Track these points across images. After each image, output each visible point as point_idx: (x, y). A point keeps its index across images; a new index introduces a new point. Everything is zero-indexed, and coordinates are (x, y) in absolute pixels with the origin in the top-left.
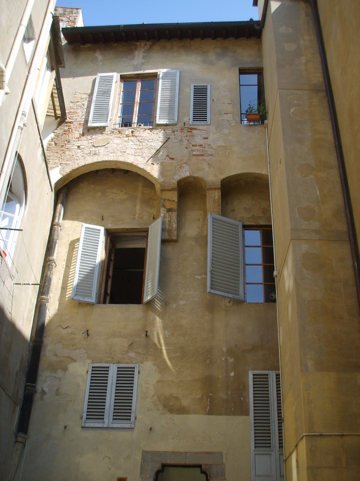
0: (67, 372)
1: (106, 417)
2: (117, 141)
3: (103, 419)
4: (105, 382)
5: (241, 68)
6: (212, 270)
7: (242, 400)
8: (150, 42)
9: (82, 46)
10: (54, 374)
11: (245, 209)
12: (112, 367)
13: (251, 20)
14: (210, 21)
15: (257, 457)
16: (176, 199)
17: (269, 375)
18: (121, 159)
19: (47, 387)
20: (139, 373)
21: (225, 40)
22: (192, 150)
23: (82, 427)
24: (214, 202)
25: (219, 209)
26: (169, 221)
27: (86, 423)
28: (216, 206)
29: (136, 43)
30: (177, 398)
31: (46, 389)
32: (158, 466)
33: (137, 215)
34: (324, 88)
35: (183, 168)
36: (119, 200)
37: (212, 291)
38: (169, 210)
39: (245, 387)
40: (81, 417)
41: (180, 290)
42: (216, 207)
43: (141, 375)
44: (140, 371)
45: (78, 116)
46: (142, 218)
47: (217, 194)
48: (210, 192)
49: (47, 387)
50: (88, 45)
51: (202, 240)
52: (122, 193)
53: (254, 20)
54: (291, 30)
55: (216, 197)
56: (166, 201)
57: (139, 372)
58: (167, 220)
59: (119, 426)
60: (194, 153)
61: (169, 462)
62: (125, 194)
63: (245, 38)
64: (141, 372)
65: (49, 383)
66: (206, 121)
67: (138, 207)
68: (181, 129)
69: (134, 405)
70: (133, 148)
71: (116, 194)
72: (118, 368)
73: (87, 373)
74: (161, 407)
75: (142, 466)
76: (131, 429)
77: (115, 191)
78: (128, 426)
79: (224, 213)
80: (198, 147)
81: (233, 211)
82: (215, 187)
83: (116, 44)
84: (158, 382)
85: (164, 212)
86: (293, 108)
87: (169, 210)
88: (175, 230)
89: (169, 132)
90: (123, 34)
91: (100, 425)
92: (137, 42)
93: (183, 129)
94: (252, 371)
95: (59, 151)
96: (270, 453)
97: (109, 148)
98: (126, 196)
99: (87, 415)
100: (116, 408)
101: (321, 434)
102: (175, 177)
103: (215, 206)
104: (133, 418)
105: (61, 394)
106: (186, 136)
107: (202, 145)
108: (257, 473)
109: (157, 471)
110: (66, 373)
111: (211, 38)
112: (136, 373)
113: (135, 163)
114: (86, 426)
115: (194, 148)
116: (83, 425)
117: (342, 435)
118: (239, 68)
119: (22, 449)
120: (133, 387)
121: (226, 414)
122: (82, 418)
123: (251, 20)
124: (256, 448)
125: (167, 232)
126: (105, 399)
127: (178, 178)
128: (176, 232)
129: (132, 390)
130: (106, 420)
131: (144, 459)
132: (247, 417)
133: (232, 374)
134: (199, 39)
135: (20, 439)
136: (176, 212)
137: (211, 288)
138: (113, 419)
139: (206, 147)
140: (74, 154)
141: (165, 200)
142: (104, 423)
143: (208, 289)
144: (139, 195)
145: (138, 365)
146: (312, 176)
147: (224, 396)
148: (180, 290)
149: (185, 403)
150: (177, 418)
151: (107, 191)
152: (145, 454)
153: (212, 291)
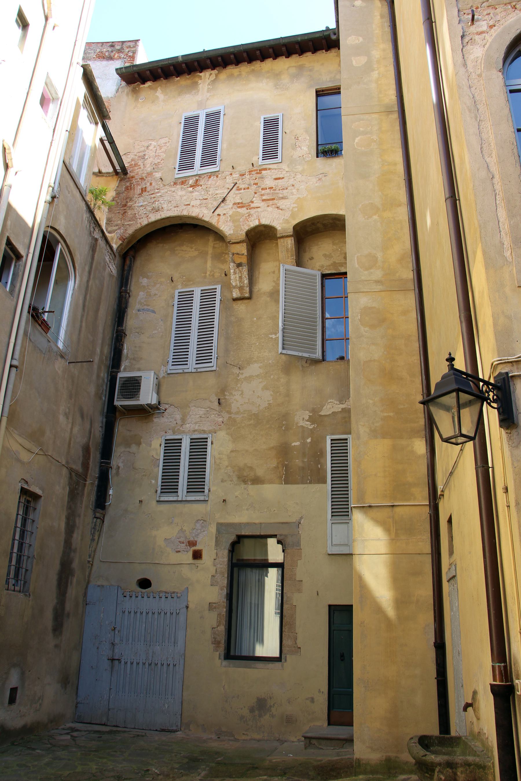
0: (141, 446)
1: (180, 491)
2: (180, 193)
3: (177, 492)
4: (178, 454)
5: (317, 89)
6: (284, 329)
7: (320, 467)
8: (215, 70)
9: (142, 86)
10: (128, 449)
11: (325, 255)
12: (185, 439)
13: (327, 28)
14: (278, 36)
15: (334, 526)
16: (245, 252)
17: (348, 439)
18: (185, 213)
19: (122, 462)
20: (212, 444)
21: (301, 56)
22: (261, 195)
23: (157, 501)
24: (287, 252)
25: (293, 259)
26: (239, 277)
27: (161, 497)
28: (289, 255)
29: (201, 74)
30: (251, 468)
31: (121, 465)
32: (233, 538)
33: (208, 273)
34: (396, 109)
35: (252, 216)
36: (190, 258)
37: (284, 352)
38: (239, 265)
39: (322, 453)
40: (156, 491)
41: (254, 351)
42: (290, 257)
43: (214, 445)
44: (213, 441)
45: (140, 168)
46: (213, 275)
47: (290, 242)
48: (282, 240)
49: (122, 462)
50: (149, 84)
51: (274, 294)
52: (193, 250)
53: (331, 28)
54: (361, 39)
55: (289, 246)
56: (235, 255)
57: (212, 442)
58: (238, 277)
59: (193, 498)
60: (264, 198)
61: (243, 534)
62: (195, 250)
63: (324, 51)
64: (214, 441)
65: (123, 458)
66: (277, 158)
67: (209, 264)
68: (250, 172)
69: (207, 476)
70: (198, 198)
71: (186, 251)
72: (191, 439)
73: (160, 446)
74: (235, 479)
75: (216, 538)
76: (205, 501)
77: (184, 248)
78: (202, 498)
79: (299, 263)
80: (268, 190)
81: (312, 259)
82: (286, 234)
83: (179, 78)
84: (232, 451)
85: (233, 268)
86: (357, 137)
87: (239, 265)
88: (246, 287)
89: (236, 176)
90: (184, 65)
91: (175, 499)
92: (201, 72)
93: (252, 171)
94: (330, 436)
95: (120, 211)
96: (348, 521)
97: (172, 202)
98: (196, 253)
99: (162, 489)
100: (189, 480)
101: (370, 505)
102: (243, 228)
103: (288, 256)
104: (206, 491)
105: (136, 469)
106: (254, 179)
107: (273, 188)
108: (334, 543)
109: (232, 542)
110: (140, 447)
111: (284, 57)
112: (209, 443)
113: (200, 216)
114: (160, 500)
115: (263, 192)
116: (158, 499)
117: (393, 506)
118: (316, 89)
119: (101, 525)
120: (206, 458)
121: (303, 483)
122: (156, 492)
123: (327, 28)
124: (334, 517)
125: (239, 289)
126: (179, 472)
127: (247, 228)
128: (248, 289)
129: (206, 461)
130: (180, 493)
131: (218, 531)
132: (324, 485)
133: (309, 440)
134: (271, 59)
135: (98, 515)
136: (247, 267)
137: (283, 348)
138: (187, 492)
139: (277, 190)
140: (137, 212)
141: (233, 254)
142: (179, 496)
143: (280, 350)
144: (210, 250)
145: (211, 435)
146: (375, 217)
147: (301, 464)
148: (254, 351)
149: (260, 472)
150: (252, 489)
151: (176, 249)
152: (220, 526)
153: (284, 352)
